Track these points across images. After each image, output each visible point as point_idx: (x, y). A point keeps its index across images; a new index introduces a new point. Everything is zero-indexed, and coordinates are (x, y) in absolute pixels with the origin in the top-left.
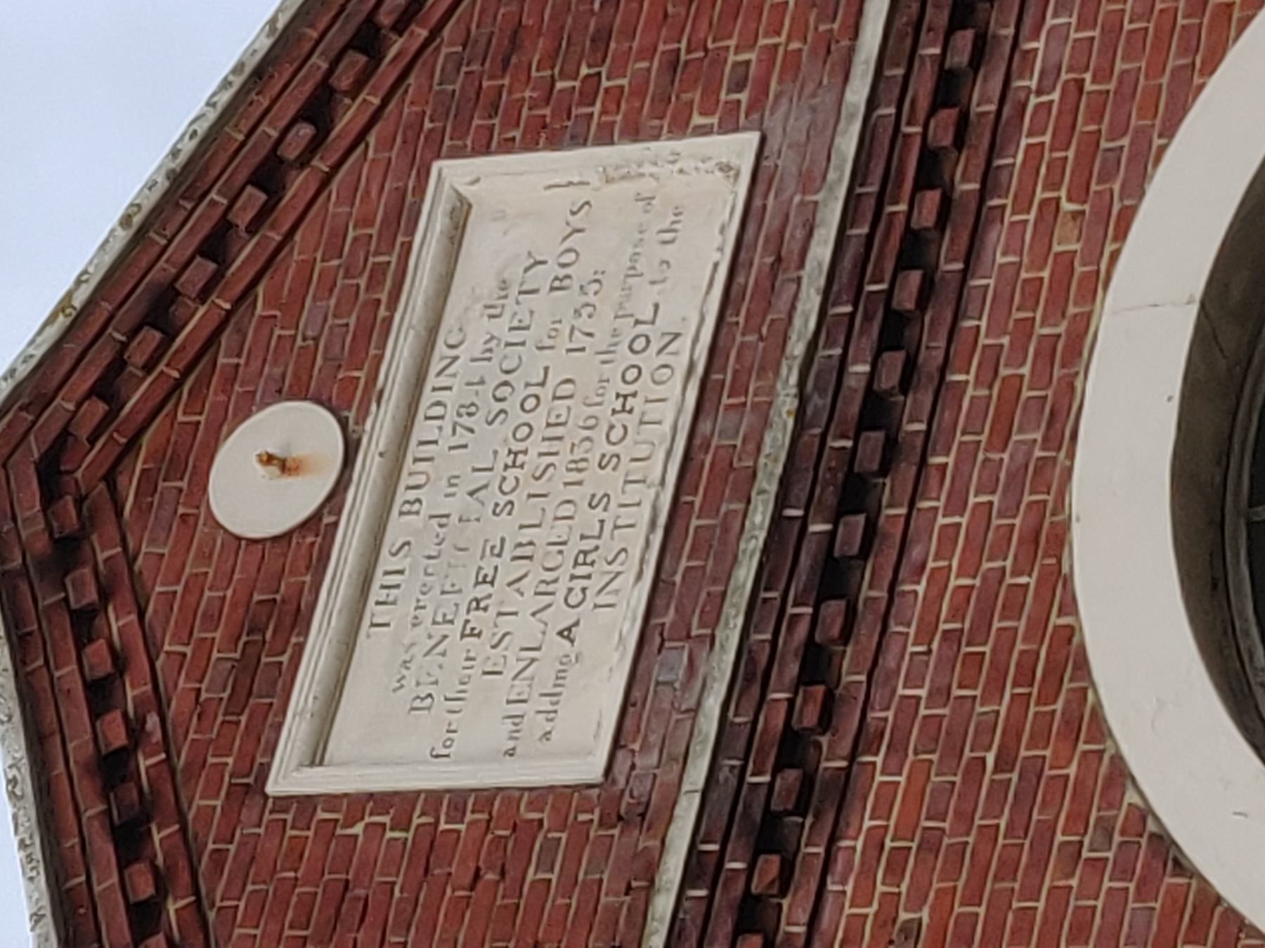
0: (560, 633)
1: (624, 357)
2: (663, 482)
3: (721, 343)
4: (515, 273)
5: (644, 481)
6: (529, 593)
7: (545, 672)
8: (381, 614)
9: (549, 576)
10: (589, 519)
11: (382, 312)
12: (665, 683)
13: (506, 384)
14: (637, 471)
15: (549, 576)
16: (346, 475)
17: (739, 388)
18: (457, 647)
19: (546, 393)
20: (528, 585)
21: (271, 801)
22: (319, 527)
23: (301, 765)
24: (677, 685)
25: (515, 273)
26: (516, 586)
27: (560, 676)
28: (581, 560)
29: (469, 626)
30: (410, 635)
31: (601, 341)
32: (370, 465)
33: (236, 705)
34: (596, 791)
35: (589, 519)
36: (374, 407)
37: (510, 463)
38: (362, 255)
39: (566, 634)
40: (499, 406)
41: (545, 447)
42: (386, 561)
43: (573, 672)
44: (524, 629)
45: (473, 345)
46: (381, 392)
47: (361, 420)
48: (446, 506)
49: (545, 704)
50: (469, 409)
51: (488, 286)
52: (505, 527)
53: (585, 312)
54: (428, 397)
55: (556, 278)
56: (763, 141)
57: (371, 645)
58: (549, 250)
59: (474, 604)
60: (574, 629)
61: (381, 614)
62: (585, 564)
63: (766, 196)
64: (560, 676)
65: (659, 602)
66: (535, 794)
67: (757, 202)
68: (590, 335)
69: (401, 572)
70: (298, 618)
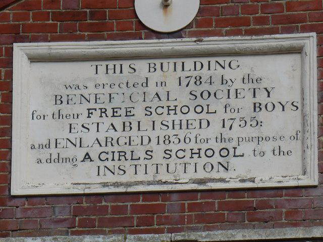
0: (87, 154)
1: (217, 147)
2: (160, 182)
3: (215, 193)
4: (264, 84)
5: (157, 173)
6: (107, 135)
7: (71, 152)
8: (101, 69)
9: (114, 142)
10: (140, 152)
11: (243, 28)
12: (54, 211)
13: (210, 94)
14: (162, 169)
15: (114, 142)
16: (166, 36)
17: (192, 208)
18: (83, 109)
19: (204, 115)
20: (112, 133)
21: (11, 46)
22: (142, 31)
23: (27, 54)
24: (53, 217)
25: (264, 84)
26: (111, 127)
27: (67, 160)
28: (121, 154)
29: (93, 111)
30: (91, 85)
31: (227, 134)
32: (168, 45)
33: (57, 16)
34: (7, 193)
35: (140, 152)
36: (194, 39)
37: (170, 108)
38: (271, 10)
39: (87, 157)
40: (199, 95)
41: (177, 122)
42: (126, 64)
43: (69, 165)
44: (89, 138)
45: (228, 74)
46: (201, 41)
47: (192, 34)
48: (152, 83)
49: (55, 156)
50: (198, 81)
51: (257, 74)
52: (139, 112)
53: (243, 123)
54: (205, 61)
55: (260, 104)
56: (315, 187)
57: (86, 69)
58: (274, 98)
59: (103, 110)
60: (89, 160)
61: (101, 69)
62: (120, 156)
63: (286, 195)
64: (67, 160)
65: (93, 198)
66: (8, 166)
67: (284, 192)
68: (231, 128)
69: (121, 72)
70: (97, 33)
